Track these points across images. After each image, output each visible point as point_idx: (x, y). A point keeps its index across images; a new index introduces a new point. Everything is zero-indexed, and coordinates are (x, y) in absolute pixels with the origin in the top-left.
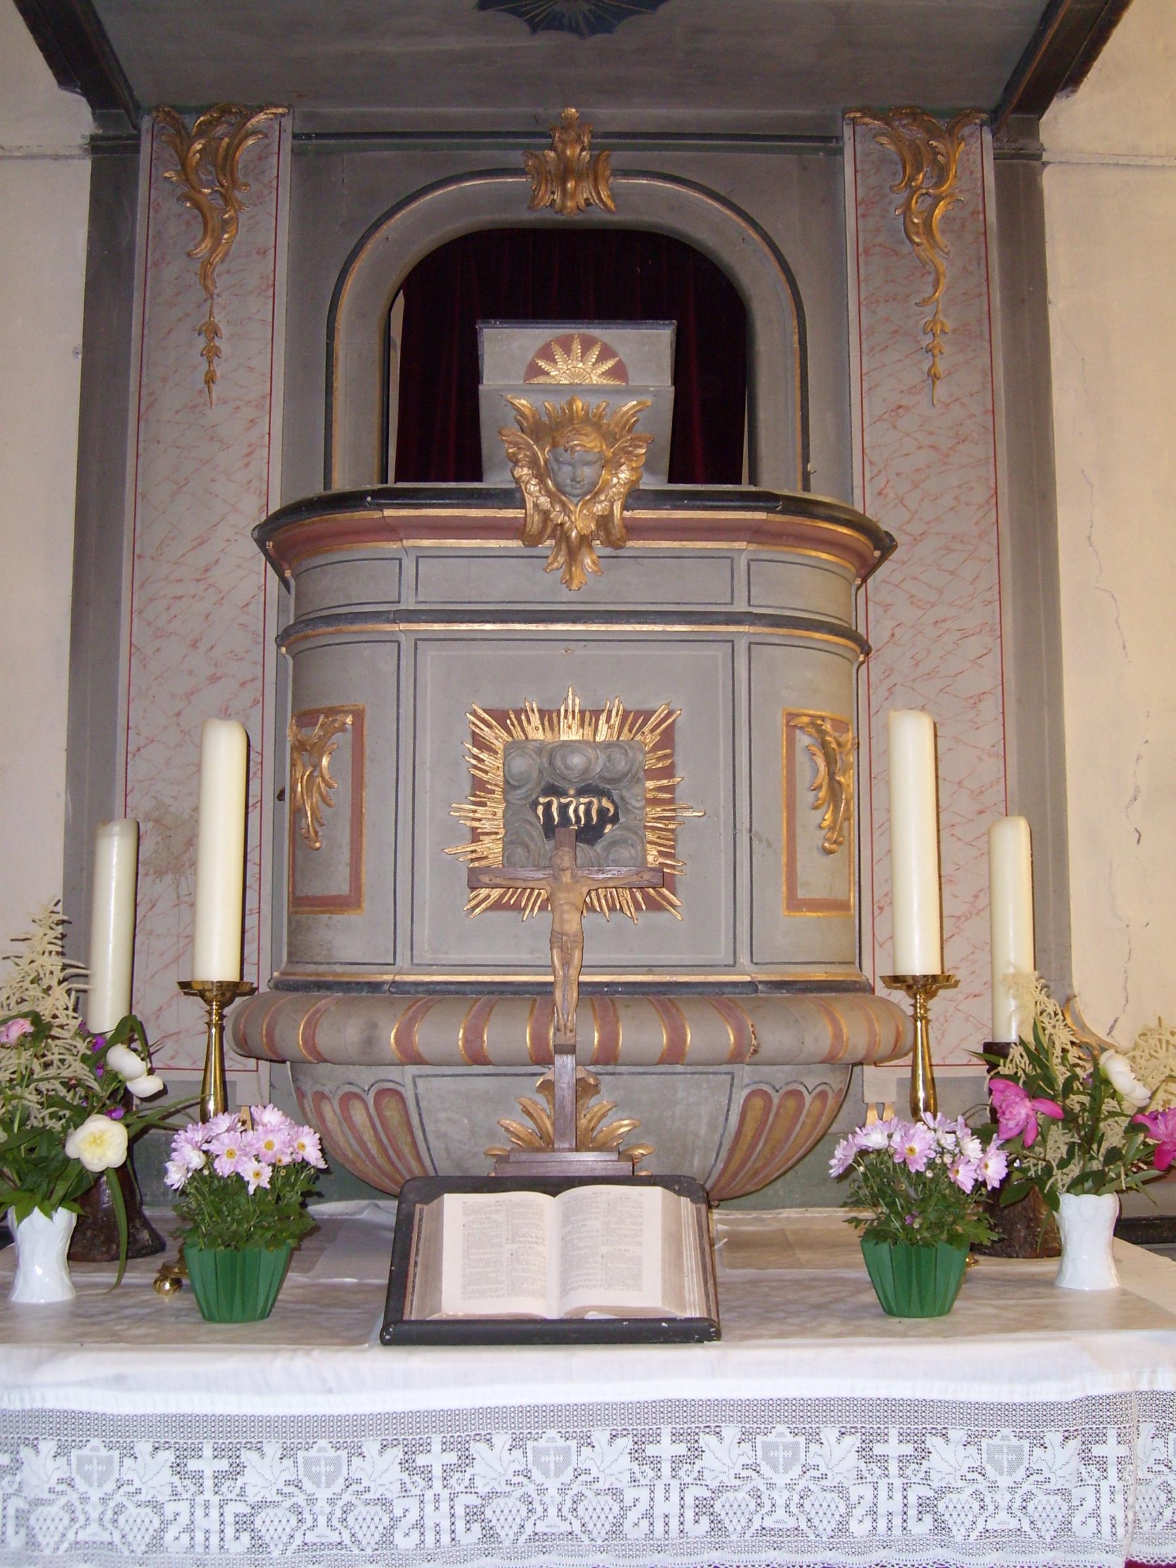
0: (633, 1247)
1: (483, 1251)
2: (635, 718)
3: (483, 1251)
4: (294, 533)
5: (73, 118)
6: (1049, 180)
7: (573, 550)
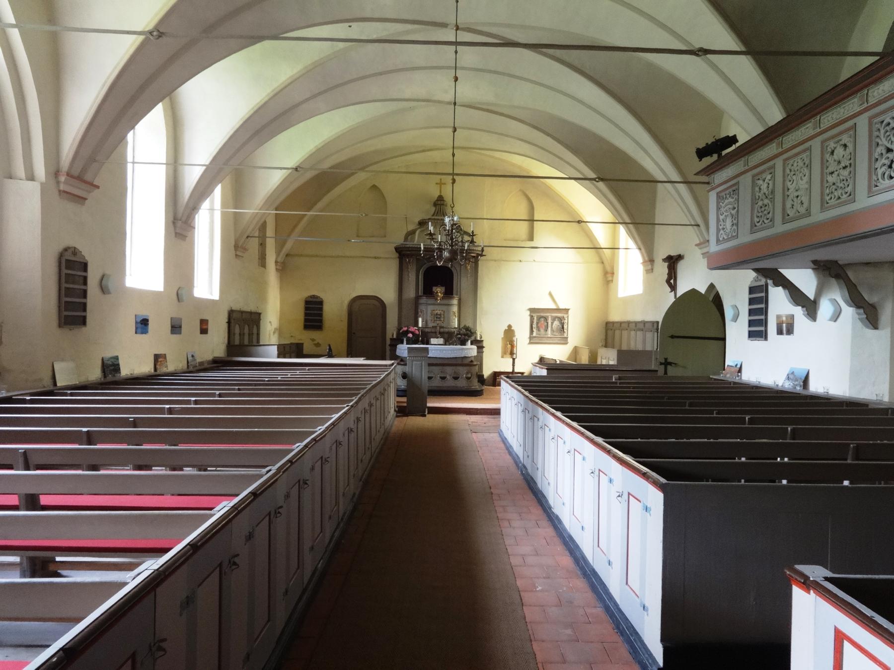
0: (441, 341)
1: (433, 341)
3: (433, 341)
4: (417, 298)
5: (397, 255)
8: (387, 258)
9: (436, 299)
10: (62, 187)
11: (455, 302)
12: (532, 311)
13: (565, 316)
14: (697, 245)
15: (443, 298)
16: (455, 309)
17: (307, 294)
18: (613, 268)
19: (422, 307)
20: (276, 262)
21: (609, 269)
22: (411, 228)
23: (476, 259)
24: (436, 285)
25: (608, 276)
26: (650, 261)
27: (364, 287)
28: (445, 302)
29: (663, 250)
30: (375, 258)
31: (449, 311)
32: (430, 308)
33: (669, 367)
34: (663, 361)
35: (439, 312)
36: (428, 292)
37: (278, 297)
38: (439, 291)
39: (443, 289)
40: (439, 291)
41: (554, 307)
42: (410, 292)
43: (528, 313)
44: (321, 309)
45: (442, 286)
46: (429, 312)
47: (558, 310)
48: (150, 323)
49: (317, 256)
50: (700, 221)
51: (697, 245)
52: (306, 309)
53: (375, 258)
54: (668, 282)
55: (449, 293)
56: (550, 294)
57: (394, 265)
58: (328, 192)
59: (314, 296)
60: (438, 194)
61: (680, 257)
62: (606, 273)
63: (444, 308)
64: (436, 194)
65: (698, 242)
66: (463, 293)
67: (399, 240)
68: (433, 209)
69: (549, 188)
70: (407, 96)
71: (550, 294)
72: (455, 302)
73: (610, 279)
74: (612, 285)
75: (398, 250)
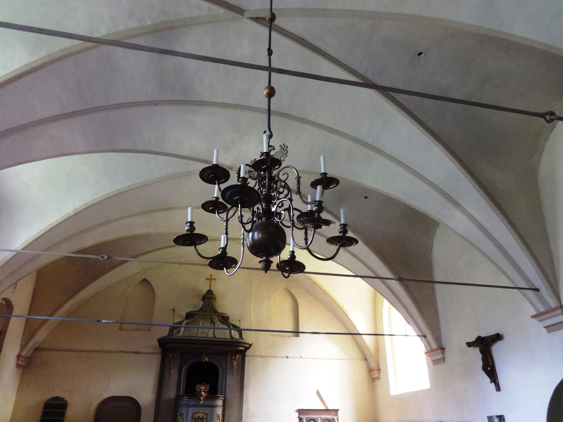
2: (205, 413)
4: (178, 397)
5: (159, 350)
6: (246, 358)
7: (201, 400)
8: (149, 353)
9: (200, 400)
10: (20, 362)
11: (220, 402)
12: (301, 412)
13: (335, 418)
14: (533, 317)
15: (206, 398)
16: (219, 411)
17: (49, 395)
18: (378, 365)
19: (183, 410)
20: (19, 356)
21: (373, 366)
22: (177, 320)
23: (243, 353)
24: (200, 383)
25: (373, 370)
26: (438, 350)
27: (118, 387)
28: (207, 403)
29: (461, 332)
30: (136, 353)
31: (212, 413)
32: (191, 410)
33: (213, 281)
34: (209, 277)
35: (201, 415)
36: (190, 391)
37: (13, 398)
38: (203, 390)
39: (208, 387)
40: (203, 390)
41: (323, 408)
42: (171, 393)
43: (297, 415)
44: (63, 414)
45: (207, 383)
46: (190, 415)
47: (327, 411)
48: (490, 415)
49: (70, 350)
50: (537, 281)
51: (533, 317)
52: (44, 414)
53: (136, 353)
54: (484, 368)
55: (213, 394)
56: (318, 393)
57: (155, 361)
58: (94, 279)
59: (57, 398)
60: (208, 288)
61: (498, 337)
62: (370, 371)
63: (207, 410)
64: (205, 289)
65: (534, 313)
66: (228, 392)
67: (164, 332)
68: (202, 303)
69: (314, 283)
70: (185, 151)
71: (318, 393)
72: (220, 402)
73: (377, 375)
74: (378, 383)
75: (162, 342)
